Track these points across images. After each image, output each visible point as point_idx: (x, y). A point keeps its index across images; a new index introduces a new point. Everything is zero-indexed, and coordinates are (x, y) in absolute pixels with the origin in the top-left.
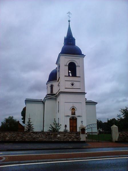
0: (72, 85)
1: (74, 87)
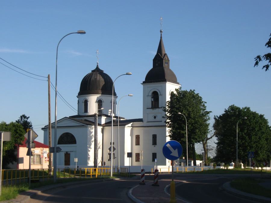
0: (155, 117)
1: (157, 119)
